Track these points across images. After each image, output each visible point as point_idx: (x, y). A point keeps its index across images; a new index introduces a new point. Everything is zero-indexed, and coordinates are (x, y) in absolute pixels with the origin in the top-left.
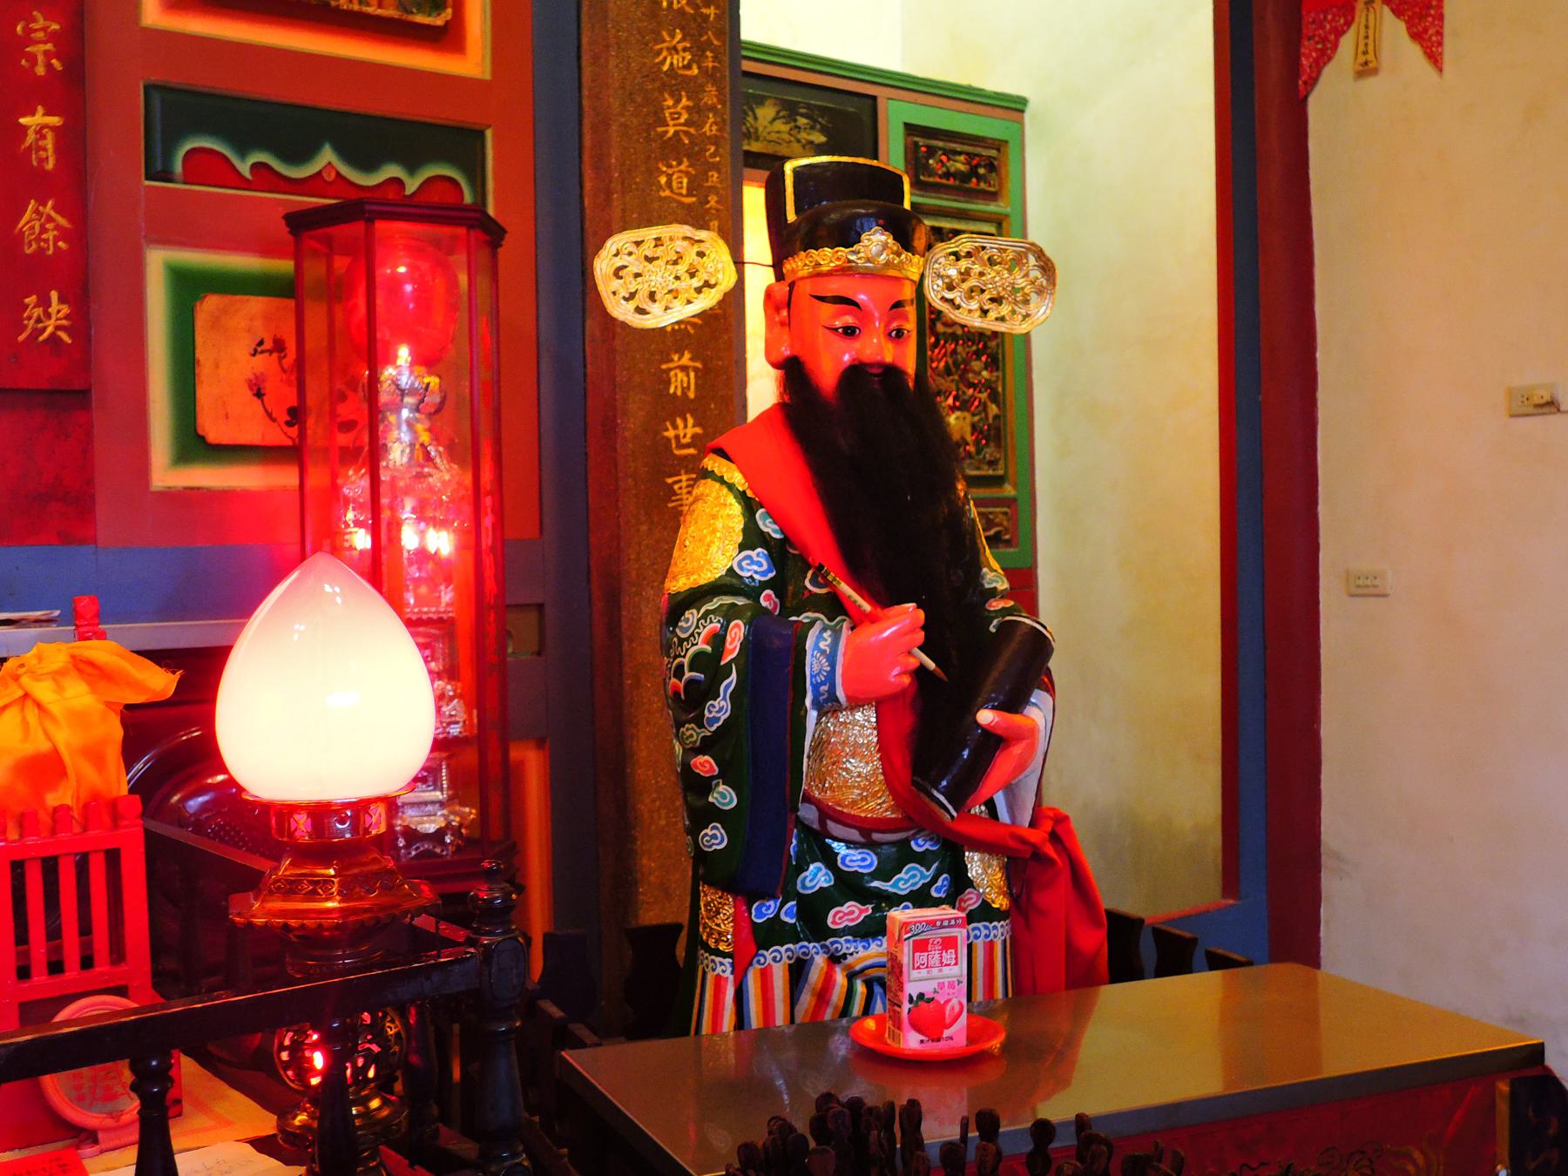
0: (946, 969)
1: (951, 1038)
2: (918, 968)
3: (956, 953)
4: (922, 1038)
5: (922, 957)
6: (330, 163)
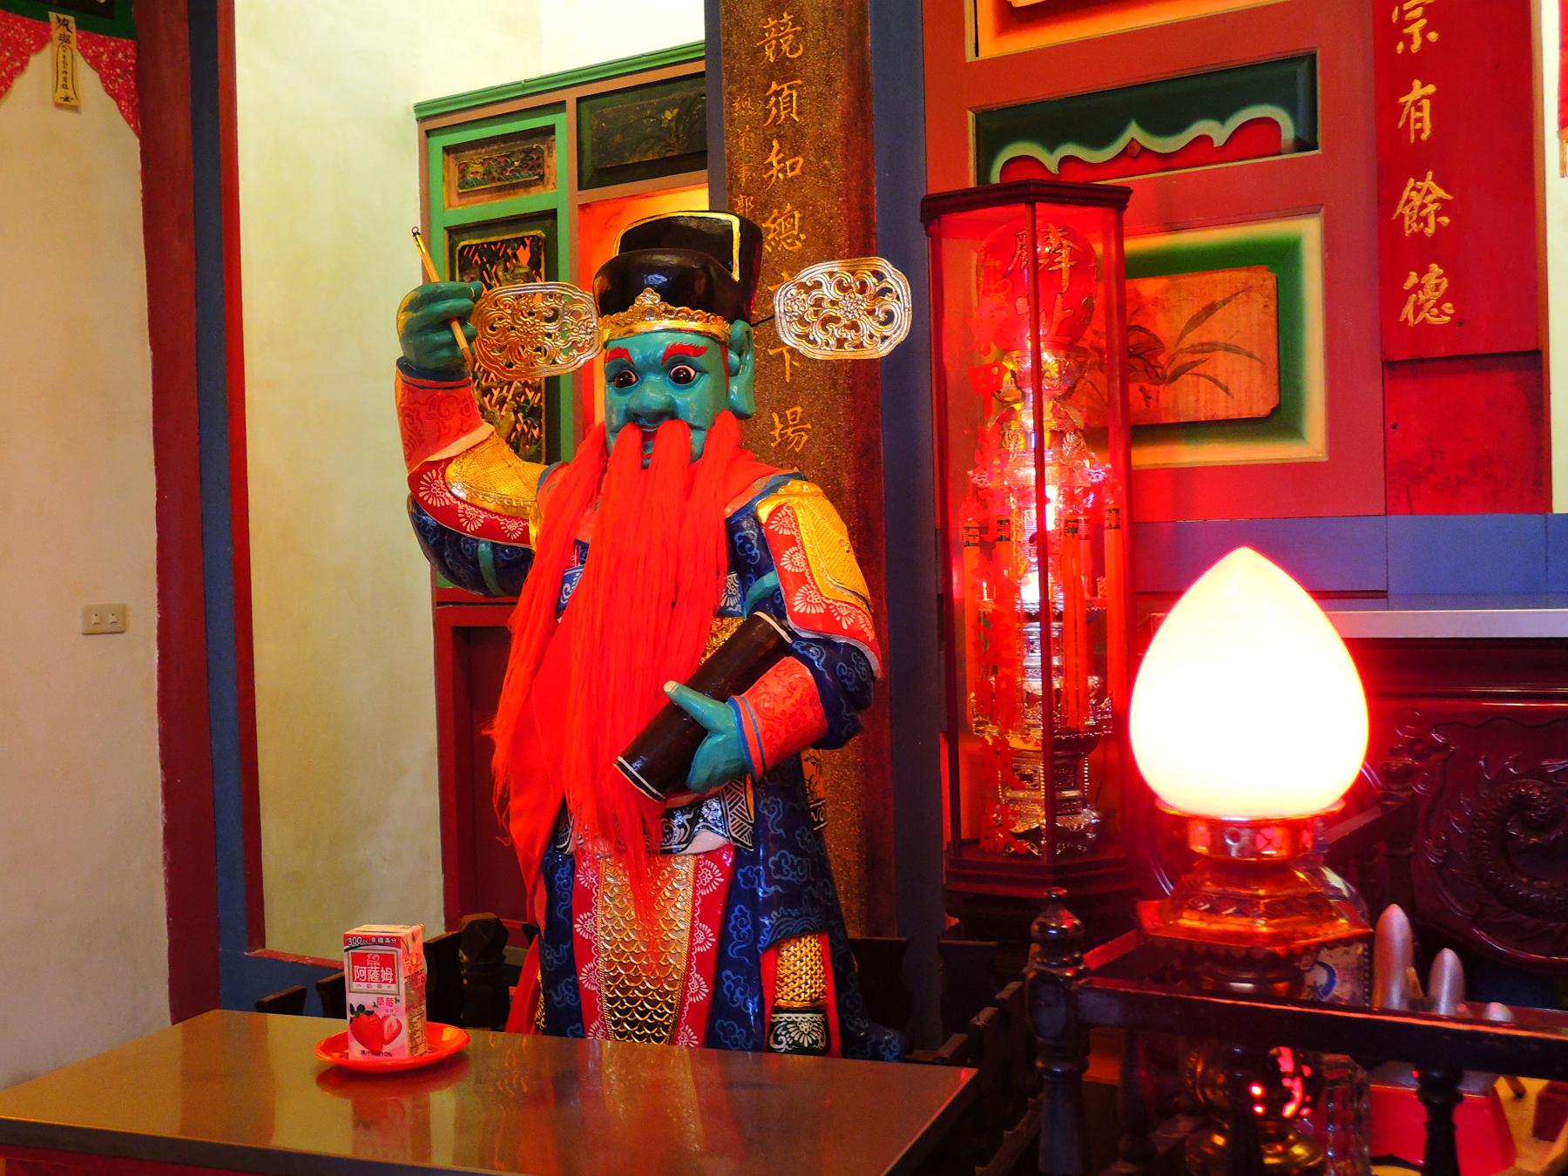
0: (385, 986)
1: (389, 1054)
2: (358, 981)
3: (393, 972)
4: (364, 1049)
5: (361, 971)
6: (1133, 139)
